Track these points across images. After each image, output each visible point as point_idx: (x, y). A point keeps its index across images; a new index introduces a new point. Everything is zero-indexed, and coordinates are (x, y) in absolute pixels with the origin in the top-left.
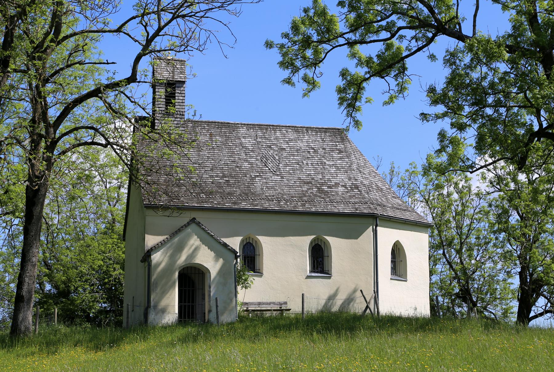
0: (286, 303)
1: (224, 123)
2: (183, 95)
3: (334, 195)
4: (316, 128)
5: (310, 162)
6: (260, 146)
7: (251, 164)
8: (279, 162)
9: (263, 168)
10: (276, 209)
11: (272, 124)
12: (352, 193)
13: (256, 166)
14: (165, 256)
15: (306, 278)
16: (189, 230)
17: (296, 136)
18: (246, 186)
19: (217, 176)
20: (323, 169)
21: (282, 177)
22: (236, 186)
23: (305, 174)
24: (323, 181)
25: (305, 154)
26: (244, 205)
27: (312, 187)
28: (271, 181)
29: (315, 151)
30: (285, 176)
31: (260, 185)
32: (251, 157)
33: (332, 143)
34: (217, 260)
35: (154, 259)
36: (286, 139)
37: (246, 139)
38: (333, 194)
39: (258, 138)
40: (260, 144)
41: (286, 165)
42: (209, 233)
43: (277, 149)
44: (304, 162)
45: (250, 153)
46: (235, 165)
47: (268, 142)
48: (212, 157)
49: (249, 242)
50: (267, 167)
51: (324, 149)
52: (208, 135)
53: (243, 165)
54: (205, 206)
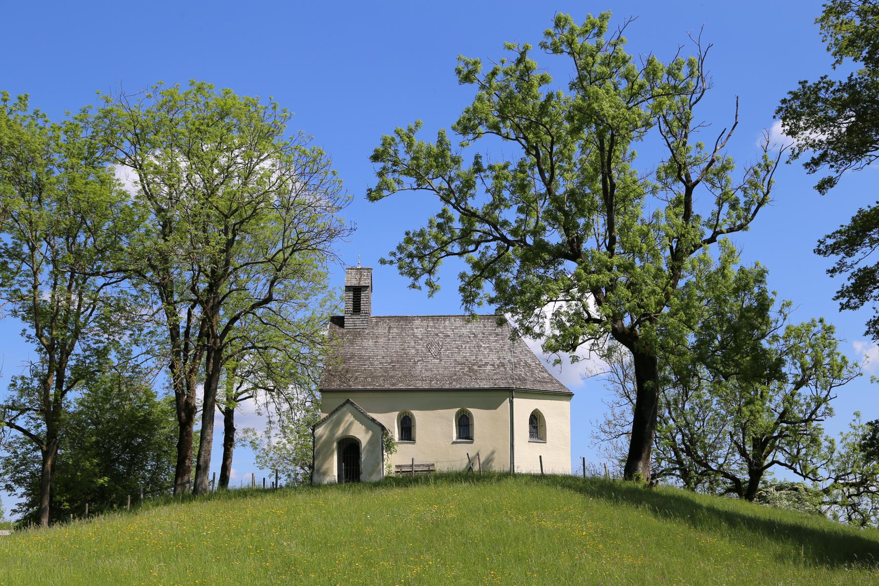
0: (433, 465)
7: (417, 350)
12: (498, 370)
16: (344, 409)
21: (441, 360)
26: (401, 386)
29: (475, 336)
34: (367, 432)
41: (447, 350)
51: (483, 333)
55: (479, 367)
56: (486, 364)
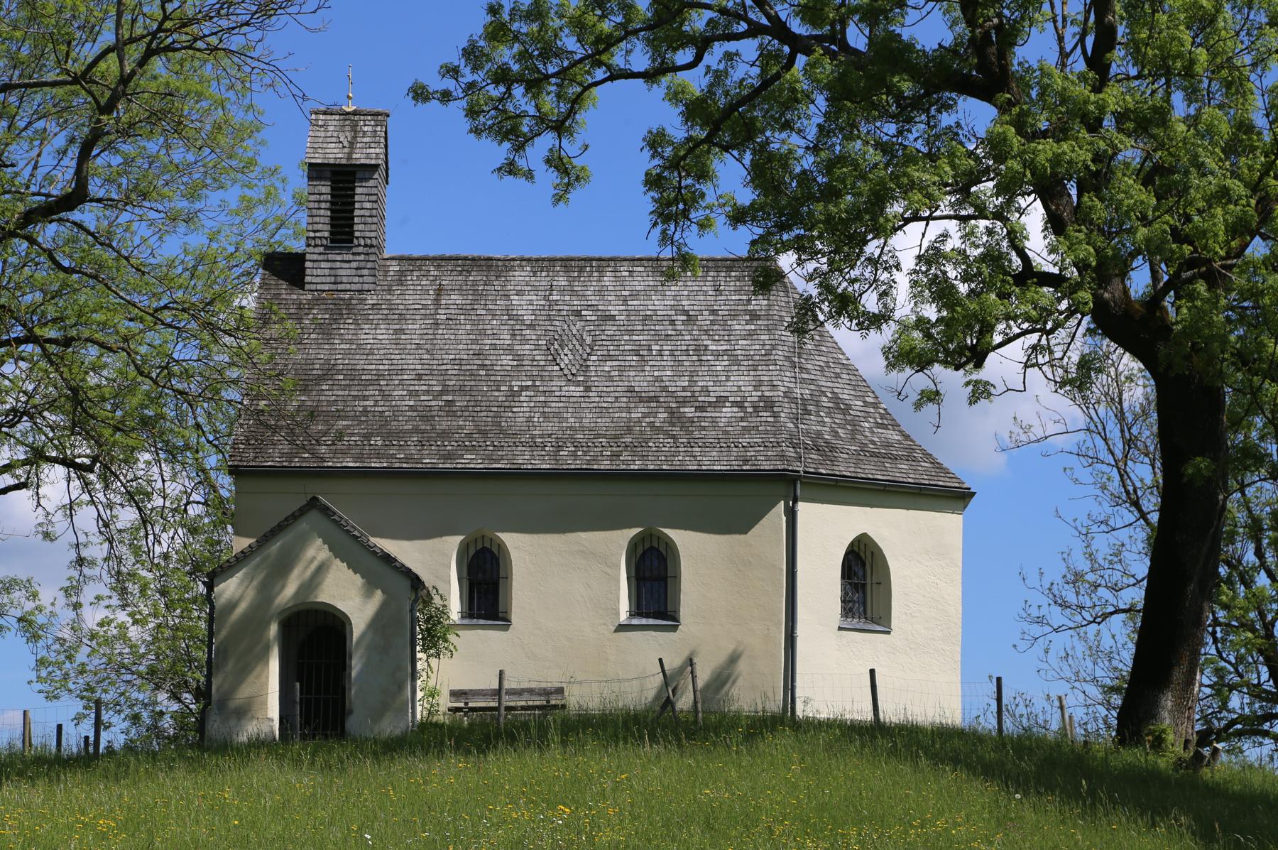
0: (560, 691)
1: (480, 259)
2: (374, 198)
3: (704, 428)
4: (708, 260)
5: (669, 348)
6: (554, 313)
7: (519, 358)
8: (588, 350)
9: (546, 368)
10: (544, 466)
11: (597, 255)
12: (754, 421)
13: (530, 363)
14: (247, 587)
15: (615, 631)
16: (303, 525)
17: (651, 283)
18: (492, 414)
19: (427, 392)
20: (697, 363)
21: (588, 389)
22: (467, 414)
23: (648, 378)
24: (689, 394)
25: (662, 328)
26: (470, 461)
27: (655, 410)
28: (557, 399)
29: (690, 319)
30: (596, 384)
31: (528, 409)
32: (525, 341)
33: (737, 297)
34: (368, 593)
35: (220, 595)
36: (623, 293)
37: (524, 298)
38: (703, 424)
39: (555, 293)
40: (556, 307)
41: (609, 357)
42: (348, 531)
43: (593, 318)
44: (653, 348)
45: (524, 332)
46: (480, 362)
47: (575, 303)
48: (426, 346)
49: (652, 548)
50: (558, 364)
51: (714, 312)
52: (431, 292)
53: (499, 363)
54: (373, 465)
55: (700, 409)
56: (721, 401)
